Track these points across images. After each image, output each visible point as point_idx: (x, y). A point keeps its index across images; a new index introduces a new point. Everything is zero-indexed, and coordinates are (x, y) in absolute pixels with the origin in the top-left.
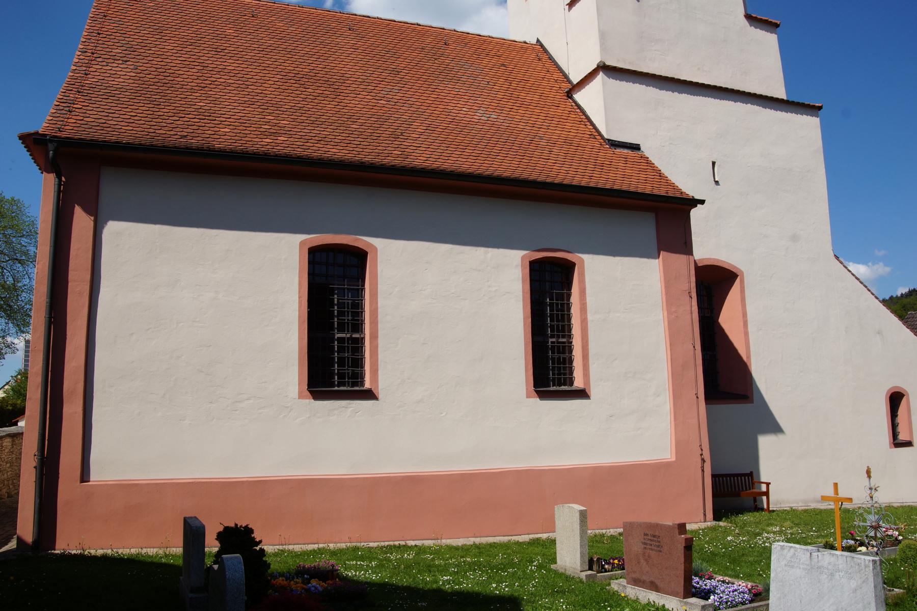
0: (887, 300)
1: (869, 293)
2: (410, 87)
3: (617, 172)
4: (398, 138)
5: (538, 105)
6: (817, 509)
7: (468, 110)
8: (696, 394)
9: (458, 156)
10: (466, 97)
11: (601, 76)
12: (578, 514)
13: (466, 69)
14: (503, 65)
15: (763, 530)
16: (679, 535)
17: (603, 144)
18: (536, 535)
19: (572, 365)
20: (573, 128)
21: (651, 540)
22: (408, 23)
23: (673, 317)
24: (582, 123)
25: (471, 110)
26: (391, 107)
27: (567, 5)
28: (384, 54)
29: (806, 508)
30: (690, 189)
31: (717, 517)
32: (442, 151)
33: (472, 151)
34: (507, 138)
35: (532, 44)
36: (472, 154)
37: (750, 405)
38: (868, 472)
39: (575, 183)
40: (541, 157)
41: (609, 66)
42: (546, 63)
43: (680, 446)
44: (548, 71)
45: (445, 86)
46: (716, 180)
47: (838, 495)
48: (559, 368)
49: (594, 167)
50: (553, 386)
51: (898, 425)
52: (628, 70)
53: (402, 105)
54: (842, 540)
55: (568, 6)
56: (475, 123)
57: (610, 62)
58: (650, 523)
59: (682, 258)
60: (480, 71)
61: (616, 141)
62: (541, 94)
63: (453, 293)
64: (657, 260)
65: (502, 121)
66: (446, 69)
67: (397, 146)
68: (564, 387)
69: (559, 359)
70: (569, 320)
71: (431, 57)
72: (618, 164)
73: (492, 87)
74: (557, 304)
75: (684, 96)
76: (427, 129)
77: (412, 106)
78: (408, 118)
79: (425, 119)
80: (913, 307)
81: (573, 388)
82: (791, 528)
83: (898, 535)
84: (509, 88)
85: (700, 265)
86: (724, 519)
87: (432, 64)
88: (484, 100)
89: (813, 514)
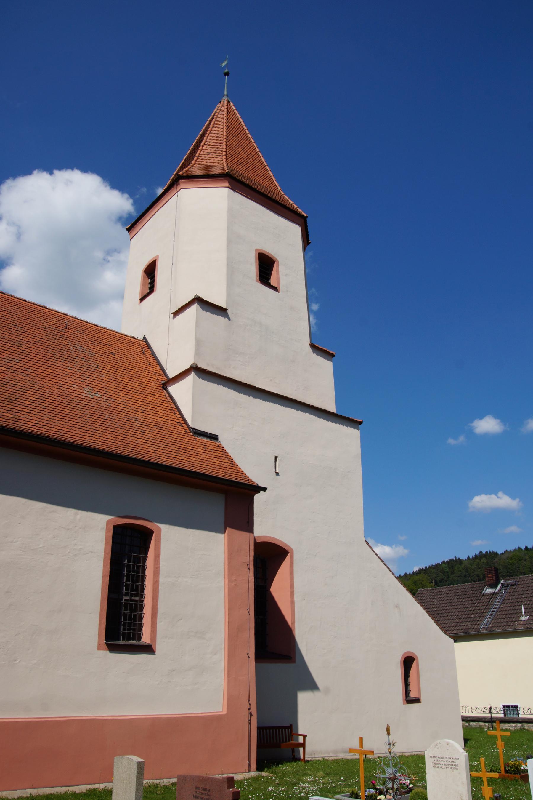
0: (402, 576)
1: (391, 573)
2: (30, 359)
3: (197, 457)
4: (12, 402)
5: (138, 391)
6: (345, 759)
7: (77, 387)
8: (248, 654)
9: (62, 426)
10: (77, 376)
11: (192, 376)
12: (135, 766)
13: (81, 352)
14: (112, 353)
15: (300, 780)
16: (228, 789)
17: (187, 431)
18: (93, 785)
19: (142, 622)
20: (164, 414)
21: (202, 794)
22: (36, 305)
23: (233, 584)
24: (172, 411)
25: (80, 387)
26: (10, 374)
27: (172, 314)
28: (11, 328)
29: (336, 758)
30: (256, 479)
31: (260, 768)
32: (49, 420)
33: (75, 423)
34: (107, 416)
35: (139, 340)
36: (75, 426)
37: (293, 664)
38: (388, 730)
39: (161, 462)
40: (135, 436)
41: (200, 368)
42: (149, 357)
43: (231, 701)
44: (149, 364)
45: (60, 363)
46: (277, 472)
47: (363, 748)
48: (130, 624)
49: (178, 450)
50: (122, 640)
51: (409, 685)
52: (215, 374)
53: (20, 374)
54: (365, 789)
55: (173, 314)
56: (82, 399)
57: (202, 365)
58: (202, 776)
59: (244, 535)
60: (92, 356)
61: (199, 430)
62: (141, 383)
63: (41, 548)
64: (223, 535)
65: (105, 401)
66: (64, 349)
67: (9, 409)
68: (133, 642)
69: (131, 615)
70: (143, 580)
71: (52, 336)
72: (199, 450)
73: (100, 370)
74: (134, 566)
75: (258, 400)
76: (38, 398)
77: (29, 376)
78: (23, 386)
79: (38, 389)
80: (421, 583)
81: (140, 643)
82: (323, 778)
83: (410, 784)
84: (115, 373)
85: (258, 541)
86: (266, 770)
87: (52, 343)
88: (92, 380)
89: (341, 764)
